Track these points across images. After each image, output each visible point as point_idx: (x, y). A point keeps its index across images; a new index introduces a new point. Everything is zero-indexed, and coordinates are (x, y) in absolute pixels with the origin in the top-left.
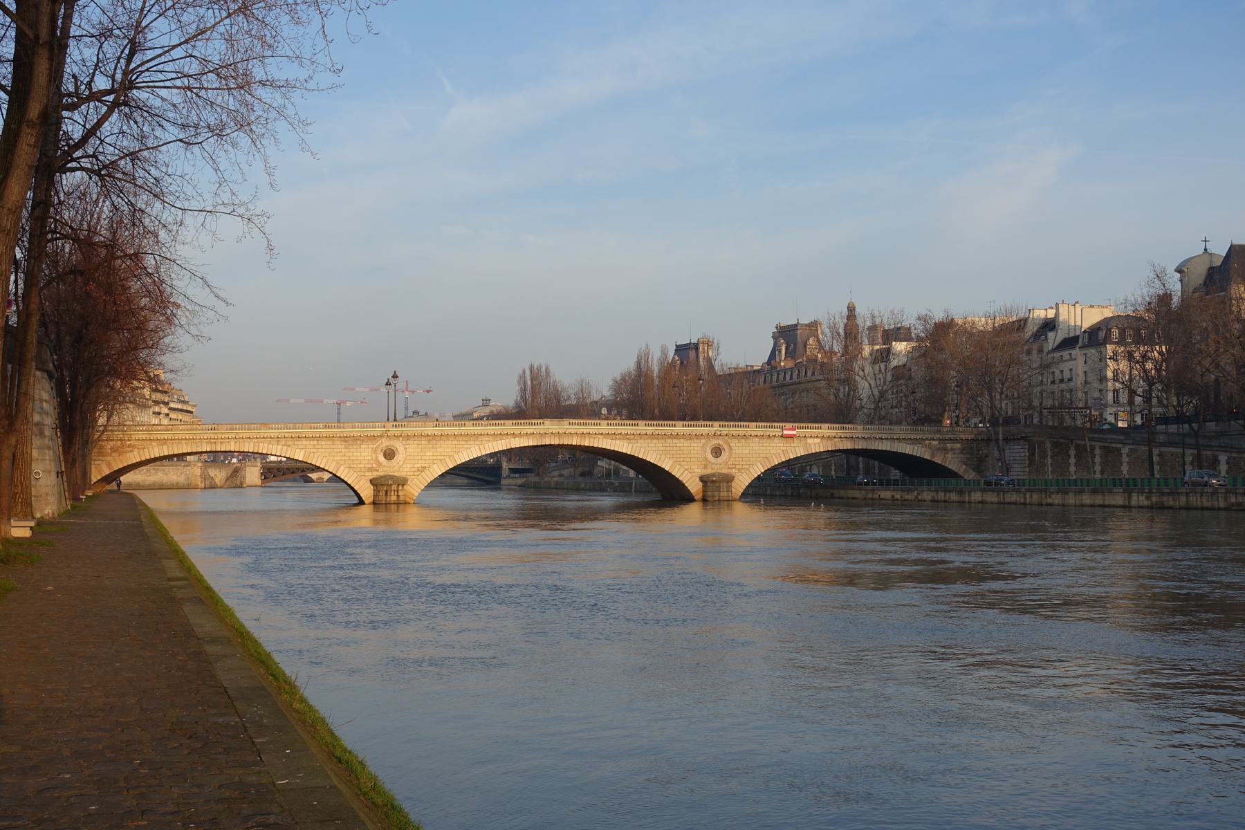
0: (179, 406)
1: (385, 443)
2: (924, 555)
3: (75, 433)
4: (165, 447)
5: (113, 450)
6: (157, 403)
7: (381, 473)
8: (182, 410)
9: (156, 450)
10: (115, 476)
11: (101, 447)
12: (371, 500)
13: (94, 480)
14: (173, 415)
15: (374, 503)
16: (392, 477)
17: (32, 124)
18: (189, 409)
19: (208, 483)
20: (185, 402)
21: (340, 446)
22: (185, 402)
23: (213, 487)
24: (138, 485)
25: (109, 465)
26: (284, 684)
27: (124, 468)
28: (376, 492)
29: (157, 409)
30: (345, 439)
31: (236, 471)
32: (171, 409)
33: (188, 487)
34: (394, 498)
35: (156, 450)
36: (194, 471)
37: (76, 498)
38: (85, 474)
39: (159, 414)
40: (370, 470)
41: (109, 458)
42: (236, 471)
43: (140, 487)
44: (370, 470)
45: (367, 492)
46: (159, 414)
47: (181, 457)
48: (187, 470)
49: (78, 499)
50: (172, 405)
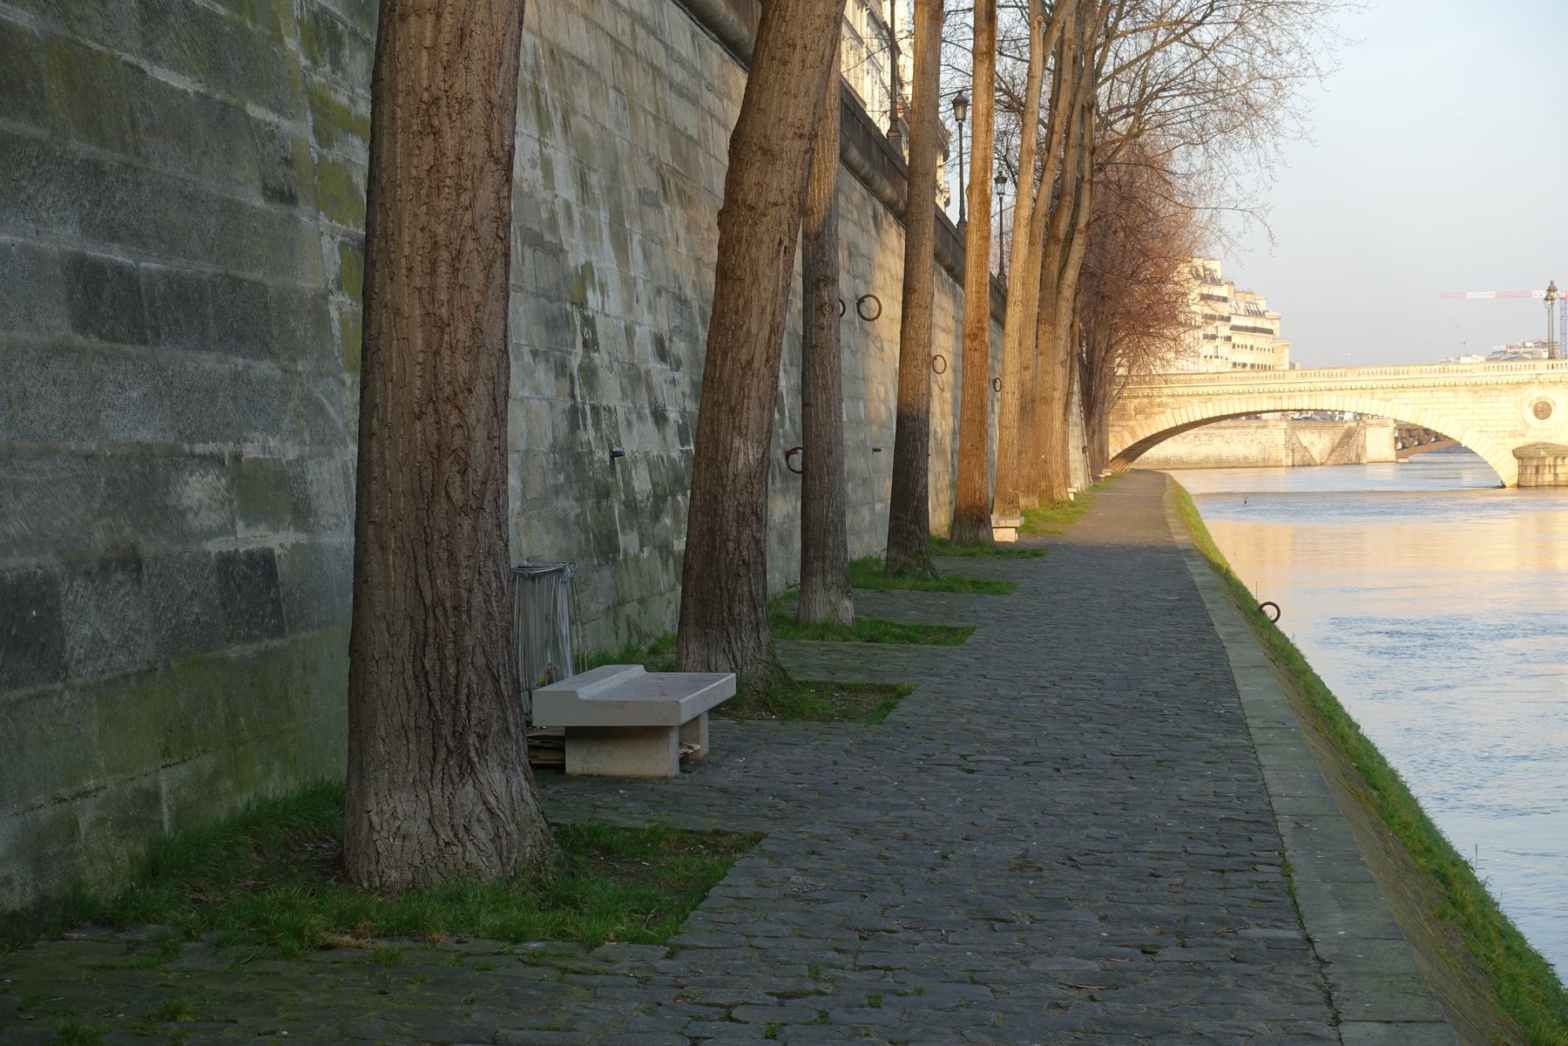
0: (1250, 322)
1: (1536, 394)
2: (589, 422)
3: (1094, 402)
4: (1210, 405)
5: (1138, 411)
6: (1210, 318)
7: (1529, 440)
8: (1254, 330)
9: (1197, 409)
10: (1132, 453)
11: (1123, 407)
12: (1515, 481)
13: (1113, 454)
14: (1238, 338)
15: (1519, 486)
16: (1545, 446)
17: (1081, 232)
18: (1267, 325)
19: (1298, 458)
20: (1259, 314)
21: (1464, 397)
22: (1259, 314)
23: (1308, 464)
24: (1181, 461)
25: (1133, 434)
26: (1339, 706)
27: (1153, 436)
28: (1523, 468)
29: (1210, 330)
30: (1474, 388)
31: (1349, 435)
32: (1234, 328)
33: (1265, 464)
34: (1548, 478)
35: (1197, 409)
36: (1273, 439)
37: (1096, 478)
38: (1103, 450)
39: (1214, 337)
40: (1513, 434)
41: (1132, 423)
42: (1349, 435)
43: (1183, 465)
44: (1513, 434)
45: (1508, 471)
46: (1214, 337)
47: (1252, 415)
48: (1262, 435)
49: (1096, 478)
50: (1235, 321)
